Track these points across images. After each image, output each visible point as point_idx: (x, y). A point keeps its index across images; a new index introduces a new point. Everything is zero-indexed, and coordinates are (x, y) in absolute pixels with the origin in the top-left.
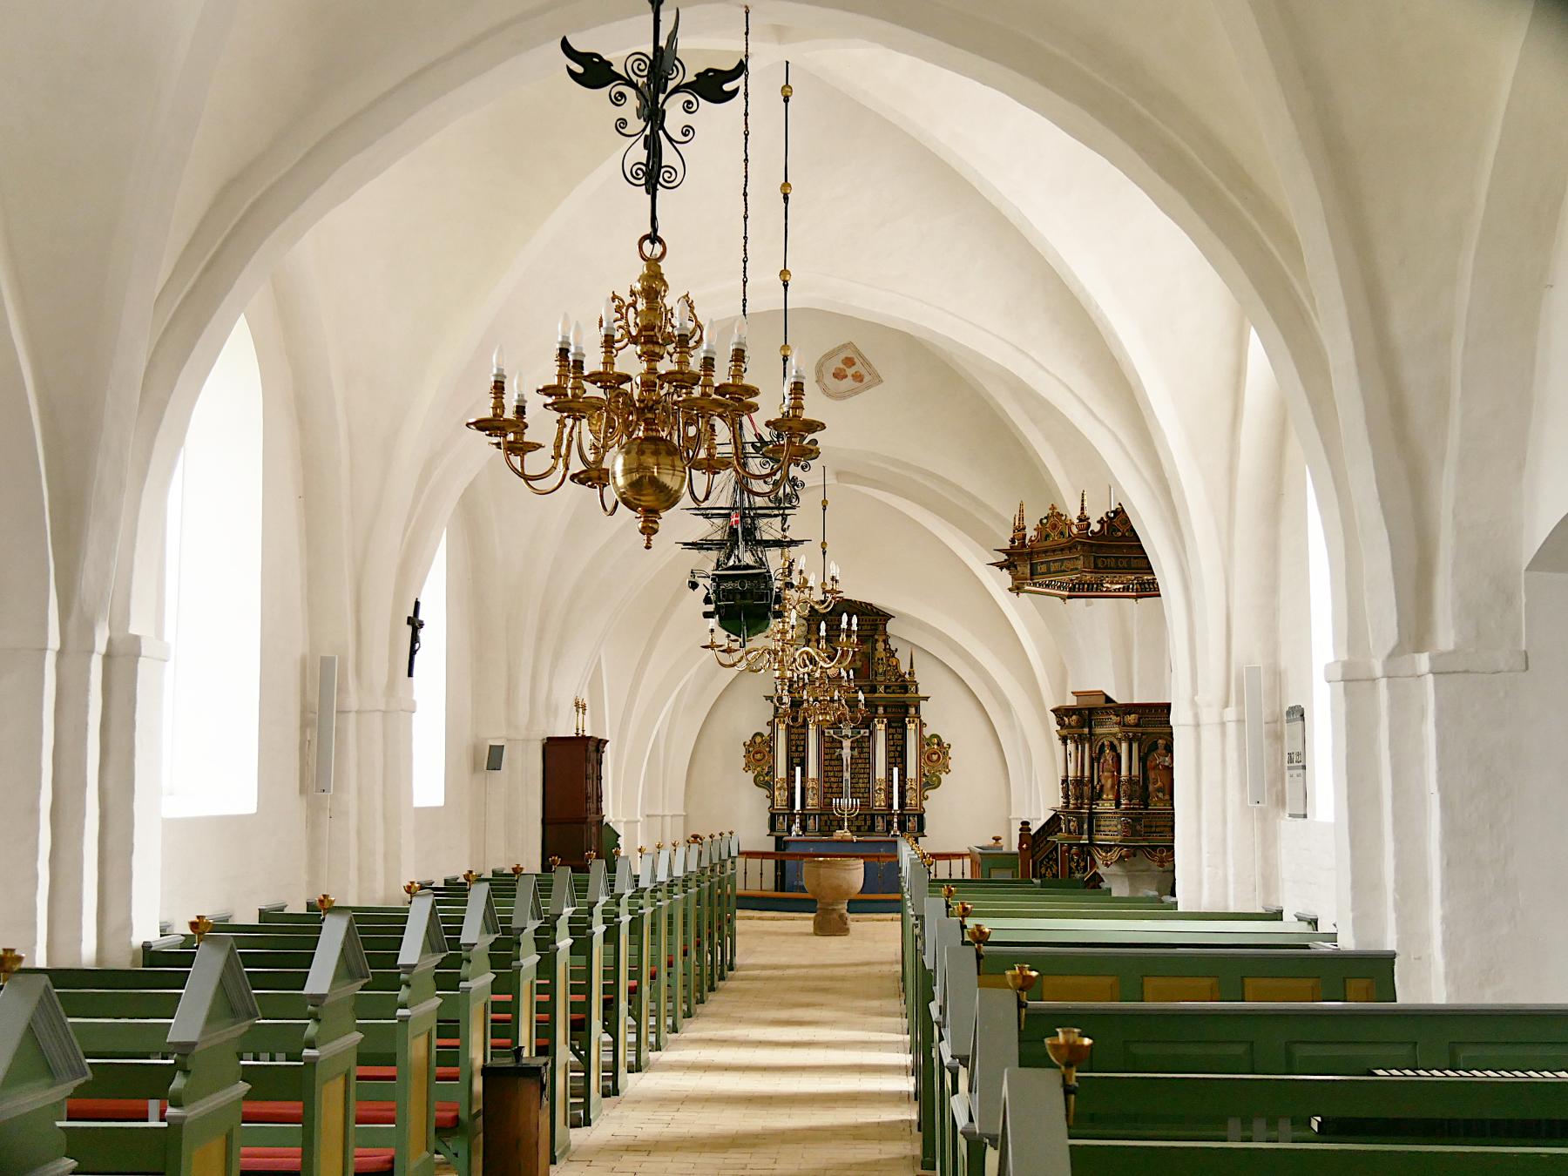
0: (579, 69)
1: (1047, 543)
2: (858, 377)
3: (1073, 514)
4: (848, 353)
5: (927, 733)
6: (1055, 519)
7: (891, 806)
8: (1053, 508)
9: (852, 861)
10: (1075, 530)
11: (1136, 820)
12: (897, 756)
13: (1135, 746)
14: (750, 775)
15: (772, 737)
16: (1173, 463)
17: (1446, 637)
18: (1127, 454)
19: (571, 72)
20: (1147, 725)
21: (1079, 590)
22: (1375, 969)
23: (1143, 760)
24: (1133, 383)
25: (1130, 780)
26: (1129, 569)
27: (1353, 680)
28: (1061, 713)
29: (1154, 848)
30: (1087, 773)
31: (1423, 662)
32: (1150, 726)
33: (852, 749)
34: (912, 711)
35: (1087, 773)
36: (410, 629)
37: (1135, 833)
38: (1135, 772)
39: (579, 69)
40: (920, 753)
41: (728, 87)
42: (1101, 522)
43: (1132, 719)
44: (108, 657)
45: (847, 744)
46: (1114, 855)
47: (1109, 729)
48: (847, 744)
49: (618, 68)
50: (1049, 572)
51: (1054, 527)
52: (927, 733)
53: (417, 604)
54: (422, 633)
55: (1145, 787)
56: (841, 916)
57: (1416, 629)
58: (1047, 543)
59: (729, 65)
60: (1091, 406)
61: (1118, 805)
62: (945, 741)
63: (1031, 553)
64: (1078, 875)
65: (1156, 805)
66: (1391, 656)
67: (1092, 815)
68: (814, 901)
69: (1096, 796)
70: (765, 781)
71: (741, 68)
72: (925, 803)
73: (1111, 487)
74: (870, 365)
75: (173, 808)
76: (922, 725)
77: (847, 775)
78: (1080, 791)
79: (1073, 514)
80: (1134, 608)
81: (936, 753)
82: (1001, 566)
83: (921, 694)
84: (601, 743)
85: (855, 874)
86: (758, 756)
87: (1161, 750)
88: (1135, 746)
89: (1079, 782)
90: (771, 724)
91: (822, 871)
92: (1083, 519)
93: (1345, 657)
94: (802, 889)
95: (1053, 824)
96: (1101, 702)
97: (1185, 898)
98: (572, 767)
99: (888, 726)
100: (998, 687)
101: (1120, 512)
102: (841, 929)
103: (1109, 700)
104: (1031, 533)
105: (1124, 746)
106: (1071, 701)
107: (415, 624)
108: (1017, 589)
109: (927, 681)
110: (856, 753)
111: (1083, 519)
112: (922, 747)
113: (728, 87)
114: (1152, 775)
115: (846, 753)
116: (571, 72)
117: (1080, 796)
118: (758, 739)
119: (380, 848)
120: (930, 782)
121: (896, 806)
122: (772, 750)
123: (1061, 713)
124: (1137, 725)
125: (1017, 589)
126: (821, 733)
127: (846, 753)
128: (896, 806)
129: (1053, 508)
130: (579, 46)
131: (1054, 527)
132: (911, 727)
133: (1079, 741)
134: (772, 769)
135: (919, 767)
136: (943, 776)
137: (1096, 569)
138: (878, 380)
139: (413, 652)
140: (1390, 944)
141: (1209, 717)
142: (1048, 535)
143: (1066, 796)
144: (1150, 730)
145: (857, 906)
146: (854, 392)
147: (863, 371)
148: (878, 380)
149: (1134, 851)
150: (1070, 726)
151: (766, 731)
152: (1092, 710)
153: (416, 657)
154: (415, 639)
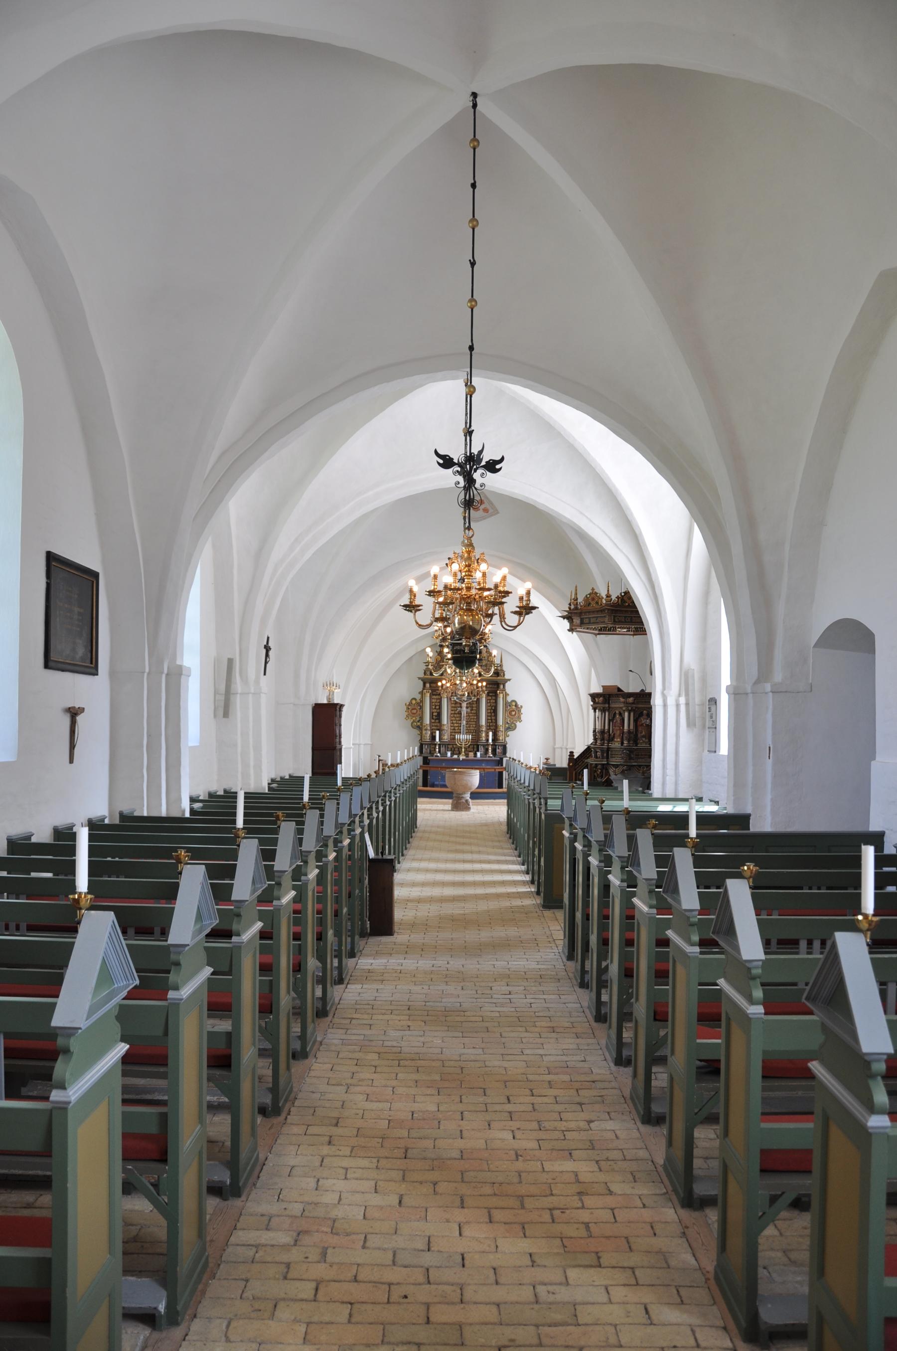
0: (441, 461)
1: (589, 608)
2: (486, 510)
3: (604, 594)
4: (491, 511)
5: (509, 699)
6: (593, 596)
7: (488, 740)
8: (593, 589)
9: (473, 771)
10: (604, 601)
11: (631, 751)
12: (493, 712)
13: (632, 714)
14: (410, 721)
15: (422, 701)
16: (668, 626)
17: (778, 676)
18: (638, 574)
19: (438, 463)
20: (638, 703)
21: (603, 631)
22: (743, 820)
23: (636, 721)
24: (637, 533)
25: (629, 732)
26: (632, 622)
27: (736, 693)
28: (594, 696)
29: (640, 766)
30: (607, 727)
31: (768, 687)
32: (641, 704)
33: (467, 708)
34: (502, 686)
35: (607, 727)
36: (264, 651)
37: (630, 758)
38: (632, 727)
39: (441, 461)
40: (505, 710)
41: (498, 467)
42: (618, 597)
43: (631, 700)
44: (167, 675)
45: (464, 705)
46: (621, 768)
47: (618, 704)
48: (464, 705)
49: (456, 461)
50: (590, 623)
51: (593, 599)
52: (509, 699)
53: (268, 638)
54: (271, 653)
55: (636, 735)
56: (467, 801)
57: (765, 673)
58: (589, 608)
59: (498, 458)
60: (615, 541)
61: (622, 743)
62: (519, 704)
63: (581, 613)
64: (599, 780)
65: (642, 745)
66: (755, 683)
67: (608, 749)
68: (451, 793)
69: (611, 739)
70: (419, 727)
71: (502, 459)
72: (507, 739)
73: (620, 577)
74: (492, 504)
75: (191, 744)
76: (507, 695)
77: (464, 723)
78: (601, 736)
79: (604, 594)
80: (632, 640)
81: (514, 710)
82: (564, 617)
83: (507, 677)
84: (342, 706)
85: (474, 778)
86: (414, 711)
87: (645, 717)
88: (632, 714)
89: (602, 732)
90: (421, 693)
91: (457, 776)
92: (608, 596)
93: (735, 684)
94: (445, 786)
95: (587, 752)
96: (616, 691)
97: (656, 789)
98: (326, 719)
99: (488, 695)
100: (495, 798)
101: (627, 593)
102: (466, 808)
103: (619, 690)
104: (580, 600)
105: (626, 714)
106: (599, 690)
107: (267, 648)
108: (571, 630)
109: (511, 671)
110: (469, 710)
111: (608, 596)
112: (506, 707)
113: (498, 467)
114: (640, 729)
115: (464, 710)
116: (438, 463)
117: (603, 739)
118: (414, 702)
119: (252, 763)
120: (511, 727)
121: (490, 741)
122: (421, 708)
123: (594, 696)
124: (633, 703)
125: (571, 630)
126: (449, 699)
127: (464, 710)
128: (490, 741)
129: (593, 589)
130: (441, 452)
131: (593, 599)
132: (501, 695)
133: (603, 711)
134: (421, 719)
135: (504, 718)
136: (518, 724)
137: (615, 622)
138: (496, 512)
139: (266, 663)
140: (748, 810)
141: (671, 701)
142: (590, 604)
143: (595, 739)
144: (640, 706)
145: (475, 796)
146: (483, 518)
147: (488, 507)
148: (496, 512)
149: (630, 768)
150: (598, 703)
151: (418, 697)
152: (610, 695)
153: (268, 665)
154: (267, 655)
